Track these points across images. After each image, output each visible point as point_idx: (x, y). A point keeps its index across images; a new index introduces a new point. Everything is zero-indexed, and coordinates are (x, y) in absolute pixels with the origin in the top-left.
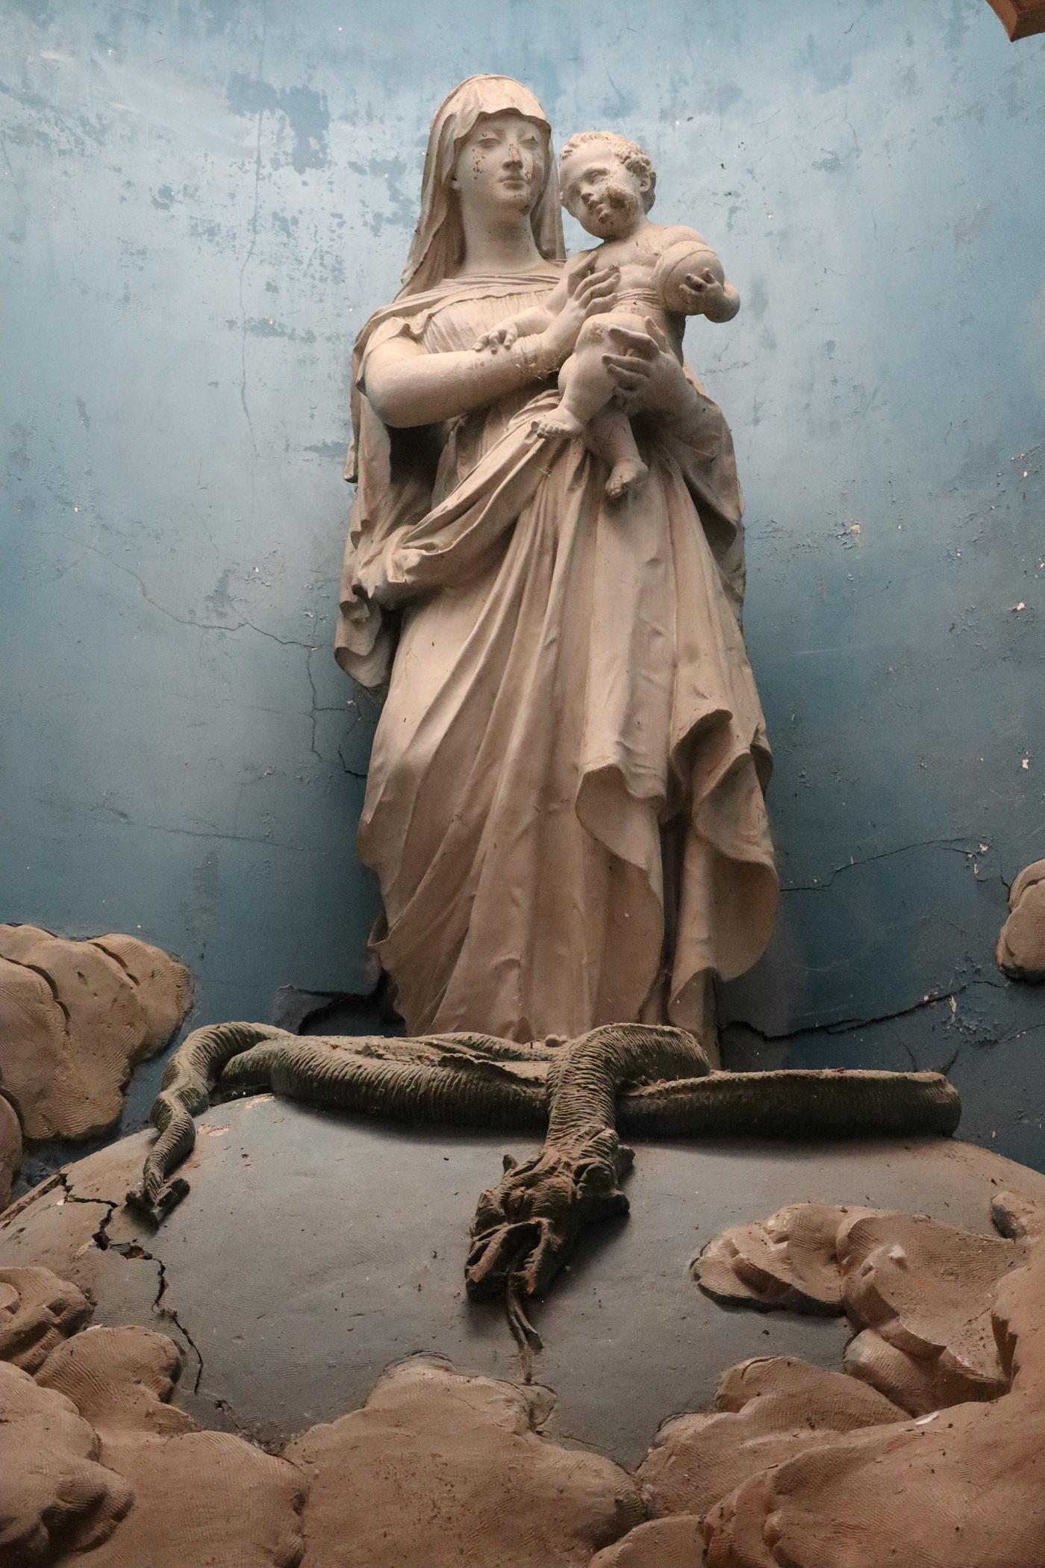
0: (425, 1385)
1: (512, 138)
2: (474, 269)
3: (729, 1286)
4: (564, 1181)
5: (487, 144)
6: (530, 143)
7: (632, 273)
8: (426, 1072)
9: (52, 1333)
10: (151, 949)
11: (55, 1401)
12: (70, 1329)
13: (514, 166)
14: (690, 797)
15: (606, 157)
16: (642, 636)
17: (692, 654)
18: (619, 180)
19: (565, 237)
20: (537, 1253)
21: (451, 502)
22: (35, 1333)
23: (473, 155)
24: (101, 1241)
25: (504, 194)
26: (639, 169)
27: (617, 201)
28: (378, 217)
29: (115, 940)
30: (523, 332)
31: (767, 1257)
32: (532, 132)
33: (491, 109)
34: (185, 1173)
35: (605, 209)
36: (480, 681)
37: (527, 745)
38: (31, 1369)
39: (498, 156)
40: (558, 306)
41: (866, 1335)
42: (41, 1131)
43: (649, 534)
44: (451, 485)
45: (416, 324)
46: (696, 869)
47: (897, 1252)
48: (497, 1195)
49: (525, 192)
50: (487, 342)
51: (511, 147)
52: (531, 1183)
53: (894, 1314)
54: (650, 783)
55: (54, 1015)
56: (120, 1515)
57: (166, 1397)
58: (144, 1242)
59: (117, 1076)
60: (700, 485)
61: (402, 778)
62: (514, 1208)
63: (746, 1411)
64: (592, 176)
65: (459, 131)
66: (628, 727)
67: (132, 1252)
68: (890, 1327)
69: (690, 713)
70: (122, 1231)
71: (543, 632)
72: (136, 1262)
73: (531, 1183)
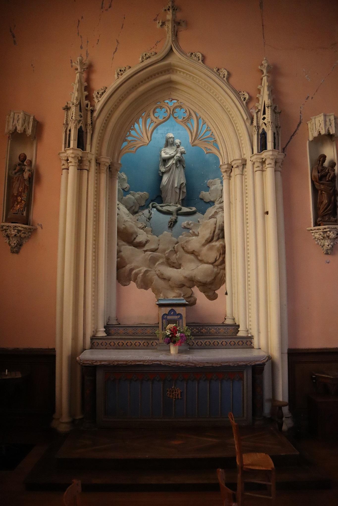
0: (166, 233)
1: (172, 139)
2: (169, 147)
3: (183, 227)
4: (174, 220)
5: (170, 139)
6: (173, 139)
7: (179, 150)
8: (166, 210)
9: (144, 228)
10: (147, 193)
11: (145, 233)
12: (145, 227)
13: (172, 141)
14: (181, 187)
15: (178, 142)
16: (179, 176)
17: (182, 178)
18: (179, 144)
19: (188, 307)
20: (172, 224)
21: (167, 166)
22: (143, 228)
23: (169, 140)
24: (147, 221)
25: (171, 142)
26: (180, 143)
27: (179, 145)
28: (162, 138)
29: (145, 192)
30: (172, 154)
31: (185, 225)
32: (173, 138)
33: (170, 137)
34: (151, 216)
35: (178, 146)
36: (169, 179)
37: (171, 184)
38: (143, 230)
39: (171, 140)
40: (174, 152)
41: (191, 230)
42: (140, 206)
43: (179, 169)
44: (167, 165)
45: (165, 151)
46: (181, 192)
47: (193, 225)
48: (170, 220)
49: (172, 142)
50: (170, 155)
51: (172, 140)
52: (172, 220)
53: (192, 229)
54: (179, 187)
55: (141, 198)
56: (149, 241)
57: (151, 233)
58: (149, 221)
59: (145, 201)
60: (183, 165)
61: (163, 186)
62: (171, 222)
63: (184, 236)
64: (177, 143)
65: (168, 138)
66: (178, 183)
67: (149, 222)
68: (192, 230)
69: (182, 182)
70: (148, 220)
71: (173, 175)
72: (149, 222)
73: (172, 220)
